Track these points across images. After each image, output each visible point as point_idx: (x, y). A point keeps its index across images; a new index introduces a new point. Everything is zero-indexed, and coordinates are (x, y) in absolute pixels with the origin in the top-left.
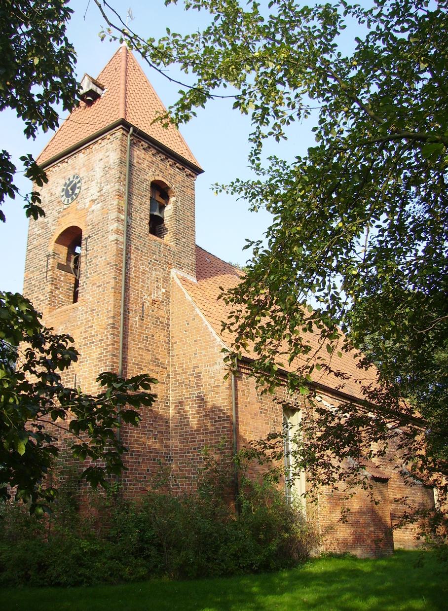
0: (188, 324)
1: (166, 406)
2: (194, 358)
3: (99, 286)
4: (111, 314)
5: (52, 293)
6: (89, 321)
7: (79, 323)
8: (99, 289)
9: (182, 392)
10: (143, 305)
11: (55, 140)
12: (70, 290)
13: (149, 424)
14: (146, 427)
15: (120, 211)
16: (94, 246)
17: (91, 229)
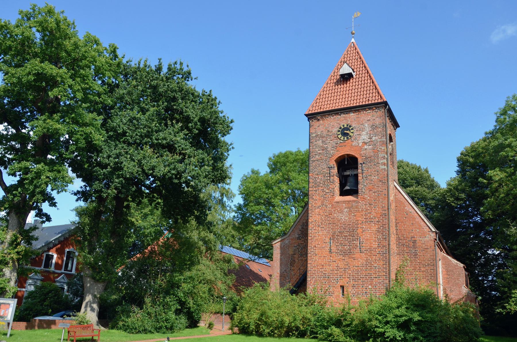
0: (407, 214)
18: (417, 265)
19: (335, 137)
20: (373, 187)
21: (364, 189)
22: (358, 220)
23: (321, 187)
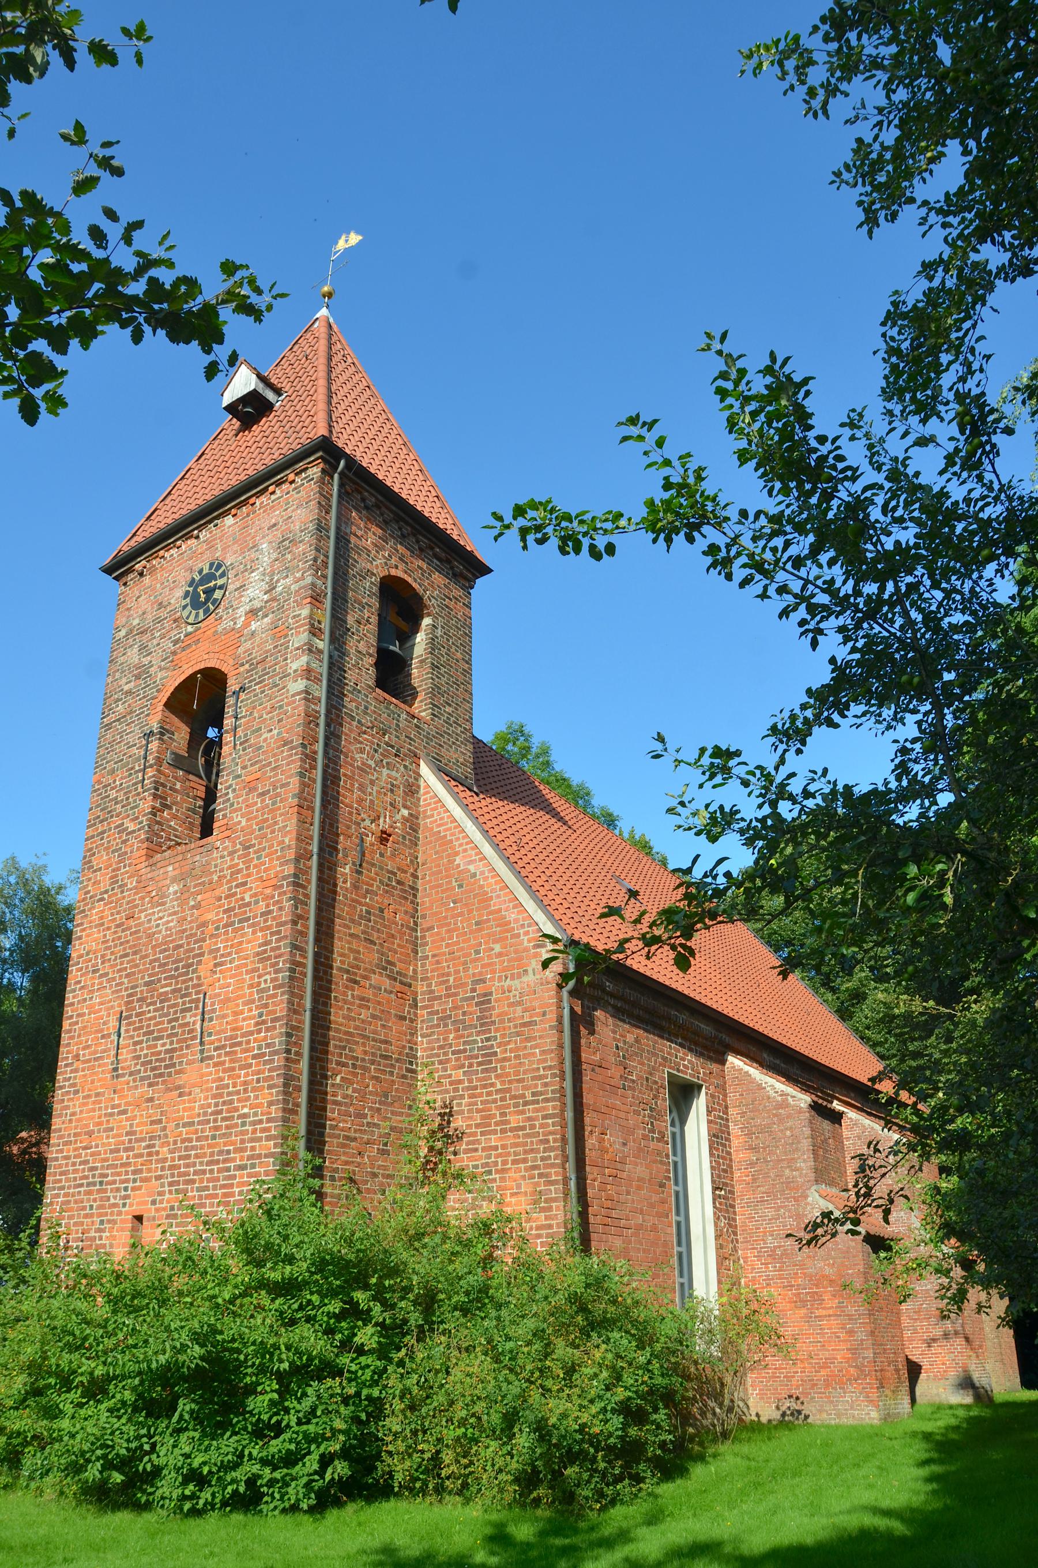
0: (460, 886)
1: (408, 1070)
2: (477, 960)
3: (263, 794)
4: (291, 855)
5: (155, 815)
6: (239, 871)
7: (215, 878)
8: (263, 801)
9: (445, 1039)
10: (362, 840)
11: (170, 498)
12: (194, 812)
13: (371, 1109)
14: (365, 1116)
15: (315, 631)
16: (254, 708)
17: (248, 671)
18: (495, 1101)
22: (204, 924)
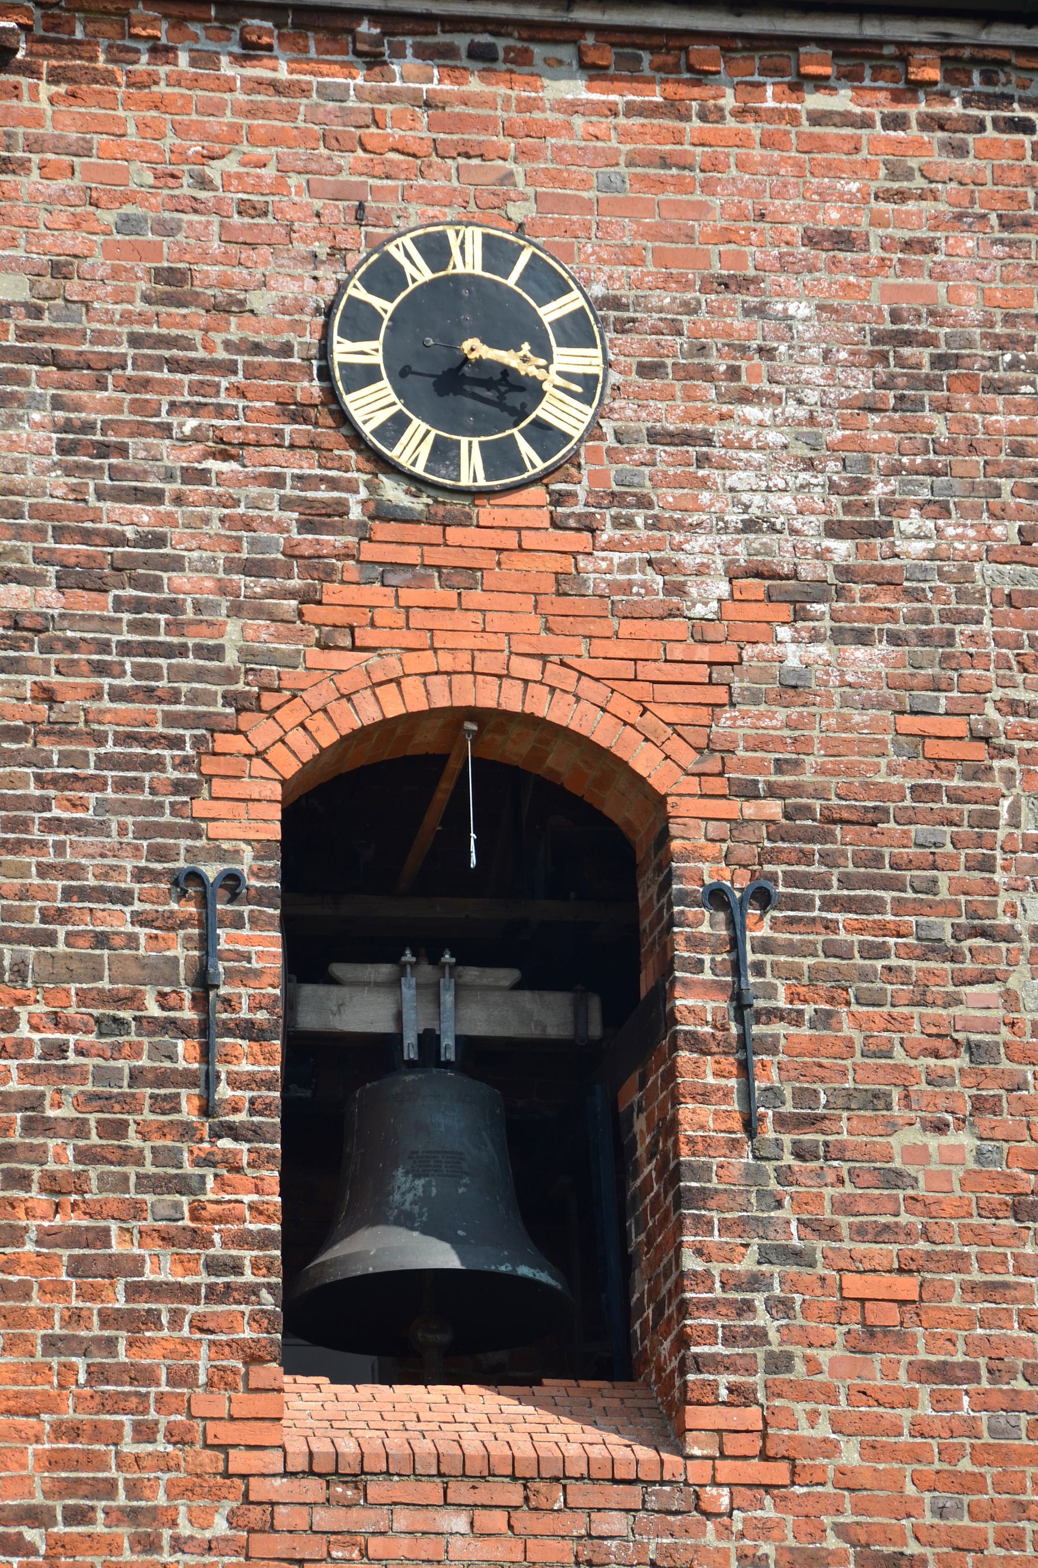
19: (298, 413)
20: (907, 1287)
21: (781, 1307)
23: (53, 1186)
